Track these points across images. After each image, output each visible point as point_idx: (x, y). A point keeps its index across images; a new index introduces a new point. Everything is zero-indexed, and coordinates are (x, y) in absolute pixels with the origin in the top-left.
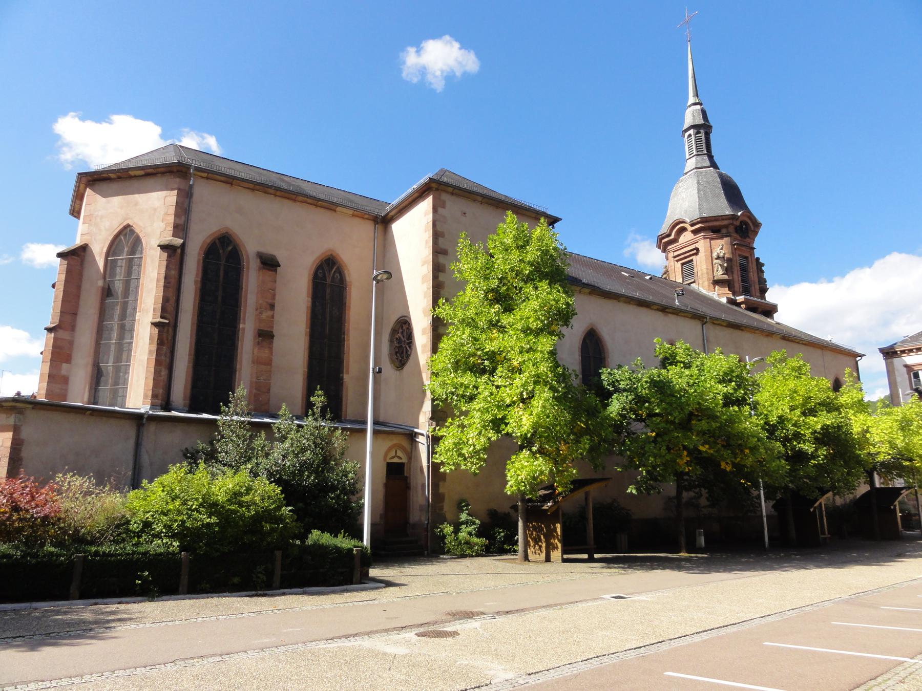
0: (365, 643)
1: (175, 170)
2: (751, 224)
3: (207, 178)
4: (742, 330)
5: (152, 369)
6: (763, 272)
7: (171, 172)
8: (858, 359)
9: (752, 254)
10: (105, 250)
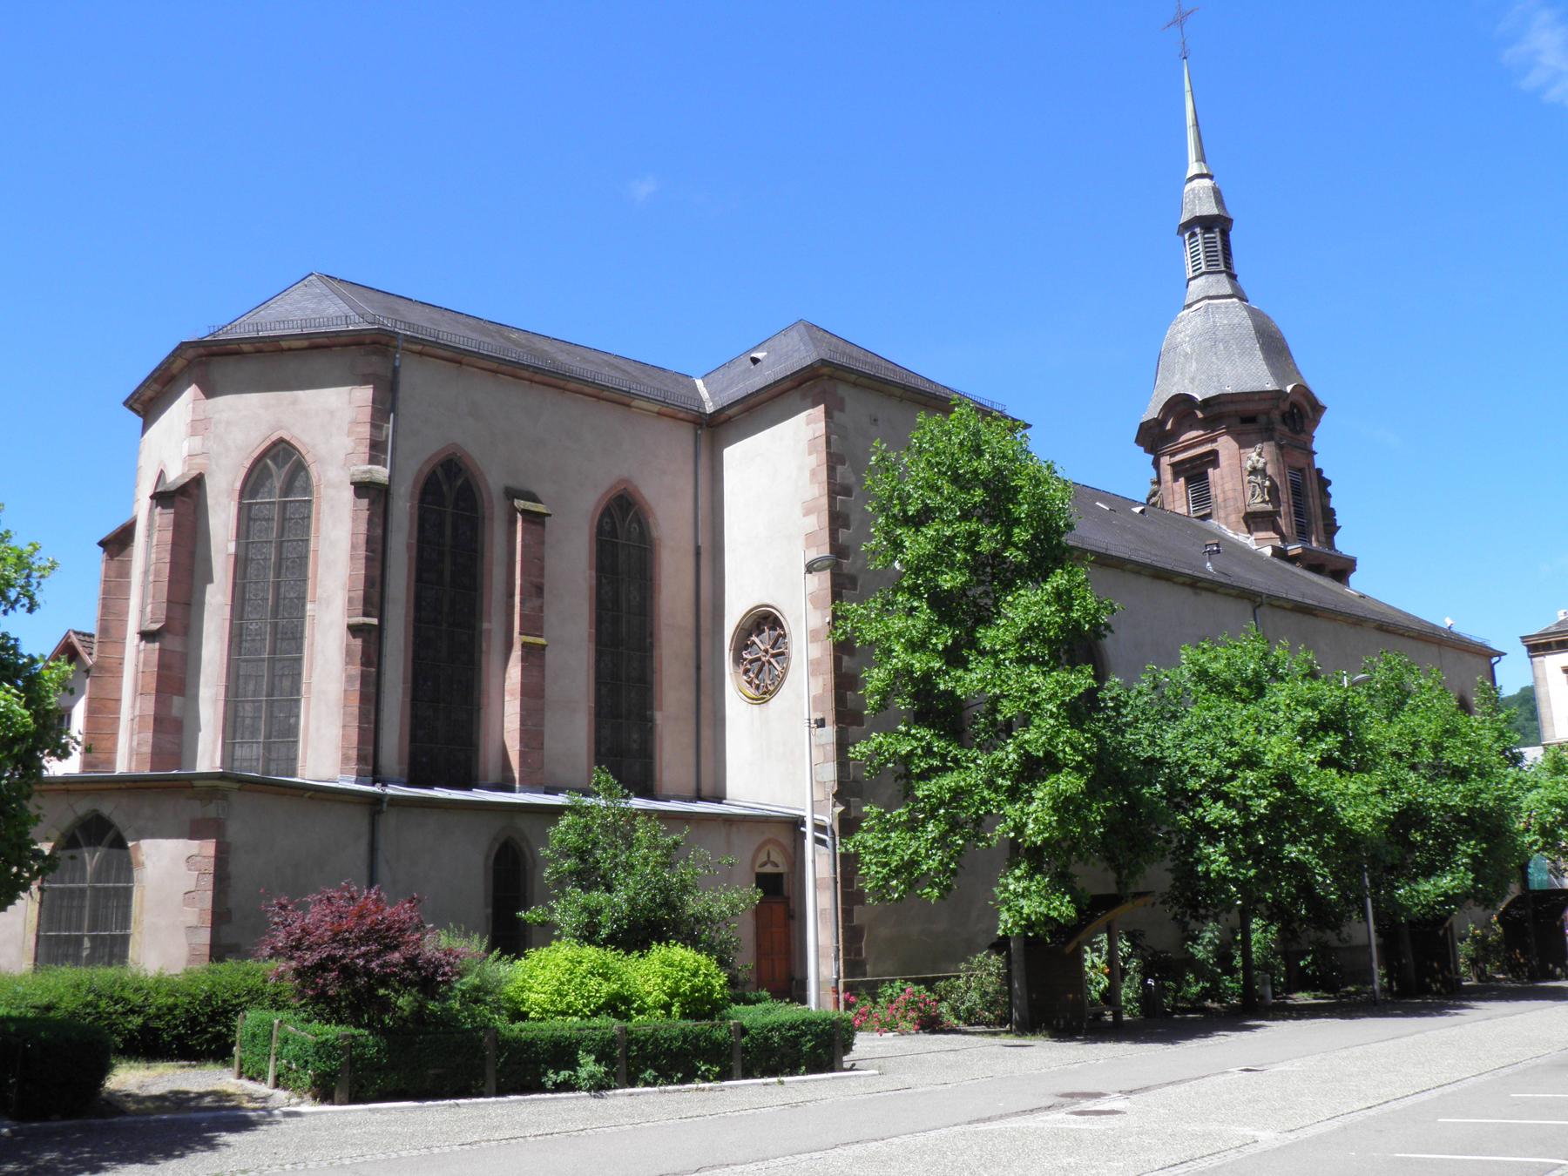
0: (995, 1126)
1: (368, 341)
2: (1308, 408)
3: (420, 353)
4: (1315, 615)
5: (356, 711)
6: (1329, 496)
7: (359, 344)
8: (1495, 659)
9: (1311, 463)
10: (238, 485)
